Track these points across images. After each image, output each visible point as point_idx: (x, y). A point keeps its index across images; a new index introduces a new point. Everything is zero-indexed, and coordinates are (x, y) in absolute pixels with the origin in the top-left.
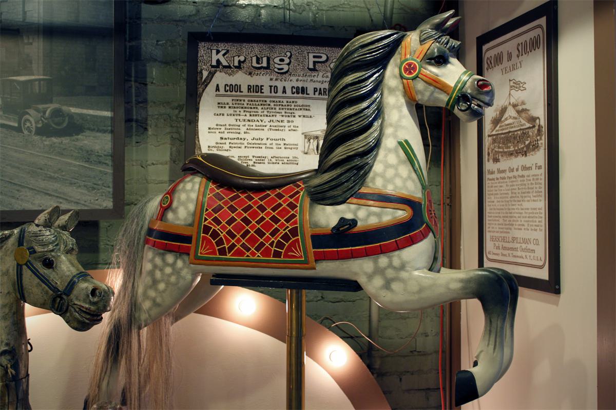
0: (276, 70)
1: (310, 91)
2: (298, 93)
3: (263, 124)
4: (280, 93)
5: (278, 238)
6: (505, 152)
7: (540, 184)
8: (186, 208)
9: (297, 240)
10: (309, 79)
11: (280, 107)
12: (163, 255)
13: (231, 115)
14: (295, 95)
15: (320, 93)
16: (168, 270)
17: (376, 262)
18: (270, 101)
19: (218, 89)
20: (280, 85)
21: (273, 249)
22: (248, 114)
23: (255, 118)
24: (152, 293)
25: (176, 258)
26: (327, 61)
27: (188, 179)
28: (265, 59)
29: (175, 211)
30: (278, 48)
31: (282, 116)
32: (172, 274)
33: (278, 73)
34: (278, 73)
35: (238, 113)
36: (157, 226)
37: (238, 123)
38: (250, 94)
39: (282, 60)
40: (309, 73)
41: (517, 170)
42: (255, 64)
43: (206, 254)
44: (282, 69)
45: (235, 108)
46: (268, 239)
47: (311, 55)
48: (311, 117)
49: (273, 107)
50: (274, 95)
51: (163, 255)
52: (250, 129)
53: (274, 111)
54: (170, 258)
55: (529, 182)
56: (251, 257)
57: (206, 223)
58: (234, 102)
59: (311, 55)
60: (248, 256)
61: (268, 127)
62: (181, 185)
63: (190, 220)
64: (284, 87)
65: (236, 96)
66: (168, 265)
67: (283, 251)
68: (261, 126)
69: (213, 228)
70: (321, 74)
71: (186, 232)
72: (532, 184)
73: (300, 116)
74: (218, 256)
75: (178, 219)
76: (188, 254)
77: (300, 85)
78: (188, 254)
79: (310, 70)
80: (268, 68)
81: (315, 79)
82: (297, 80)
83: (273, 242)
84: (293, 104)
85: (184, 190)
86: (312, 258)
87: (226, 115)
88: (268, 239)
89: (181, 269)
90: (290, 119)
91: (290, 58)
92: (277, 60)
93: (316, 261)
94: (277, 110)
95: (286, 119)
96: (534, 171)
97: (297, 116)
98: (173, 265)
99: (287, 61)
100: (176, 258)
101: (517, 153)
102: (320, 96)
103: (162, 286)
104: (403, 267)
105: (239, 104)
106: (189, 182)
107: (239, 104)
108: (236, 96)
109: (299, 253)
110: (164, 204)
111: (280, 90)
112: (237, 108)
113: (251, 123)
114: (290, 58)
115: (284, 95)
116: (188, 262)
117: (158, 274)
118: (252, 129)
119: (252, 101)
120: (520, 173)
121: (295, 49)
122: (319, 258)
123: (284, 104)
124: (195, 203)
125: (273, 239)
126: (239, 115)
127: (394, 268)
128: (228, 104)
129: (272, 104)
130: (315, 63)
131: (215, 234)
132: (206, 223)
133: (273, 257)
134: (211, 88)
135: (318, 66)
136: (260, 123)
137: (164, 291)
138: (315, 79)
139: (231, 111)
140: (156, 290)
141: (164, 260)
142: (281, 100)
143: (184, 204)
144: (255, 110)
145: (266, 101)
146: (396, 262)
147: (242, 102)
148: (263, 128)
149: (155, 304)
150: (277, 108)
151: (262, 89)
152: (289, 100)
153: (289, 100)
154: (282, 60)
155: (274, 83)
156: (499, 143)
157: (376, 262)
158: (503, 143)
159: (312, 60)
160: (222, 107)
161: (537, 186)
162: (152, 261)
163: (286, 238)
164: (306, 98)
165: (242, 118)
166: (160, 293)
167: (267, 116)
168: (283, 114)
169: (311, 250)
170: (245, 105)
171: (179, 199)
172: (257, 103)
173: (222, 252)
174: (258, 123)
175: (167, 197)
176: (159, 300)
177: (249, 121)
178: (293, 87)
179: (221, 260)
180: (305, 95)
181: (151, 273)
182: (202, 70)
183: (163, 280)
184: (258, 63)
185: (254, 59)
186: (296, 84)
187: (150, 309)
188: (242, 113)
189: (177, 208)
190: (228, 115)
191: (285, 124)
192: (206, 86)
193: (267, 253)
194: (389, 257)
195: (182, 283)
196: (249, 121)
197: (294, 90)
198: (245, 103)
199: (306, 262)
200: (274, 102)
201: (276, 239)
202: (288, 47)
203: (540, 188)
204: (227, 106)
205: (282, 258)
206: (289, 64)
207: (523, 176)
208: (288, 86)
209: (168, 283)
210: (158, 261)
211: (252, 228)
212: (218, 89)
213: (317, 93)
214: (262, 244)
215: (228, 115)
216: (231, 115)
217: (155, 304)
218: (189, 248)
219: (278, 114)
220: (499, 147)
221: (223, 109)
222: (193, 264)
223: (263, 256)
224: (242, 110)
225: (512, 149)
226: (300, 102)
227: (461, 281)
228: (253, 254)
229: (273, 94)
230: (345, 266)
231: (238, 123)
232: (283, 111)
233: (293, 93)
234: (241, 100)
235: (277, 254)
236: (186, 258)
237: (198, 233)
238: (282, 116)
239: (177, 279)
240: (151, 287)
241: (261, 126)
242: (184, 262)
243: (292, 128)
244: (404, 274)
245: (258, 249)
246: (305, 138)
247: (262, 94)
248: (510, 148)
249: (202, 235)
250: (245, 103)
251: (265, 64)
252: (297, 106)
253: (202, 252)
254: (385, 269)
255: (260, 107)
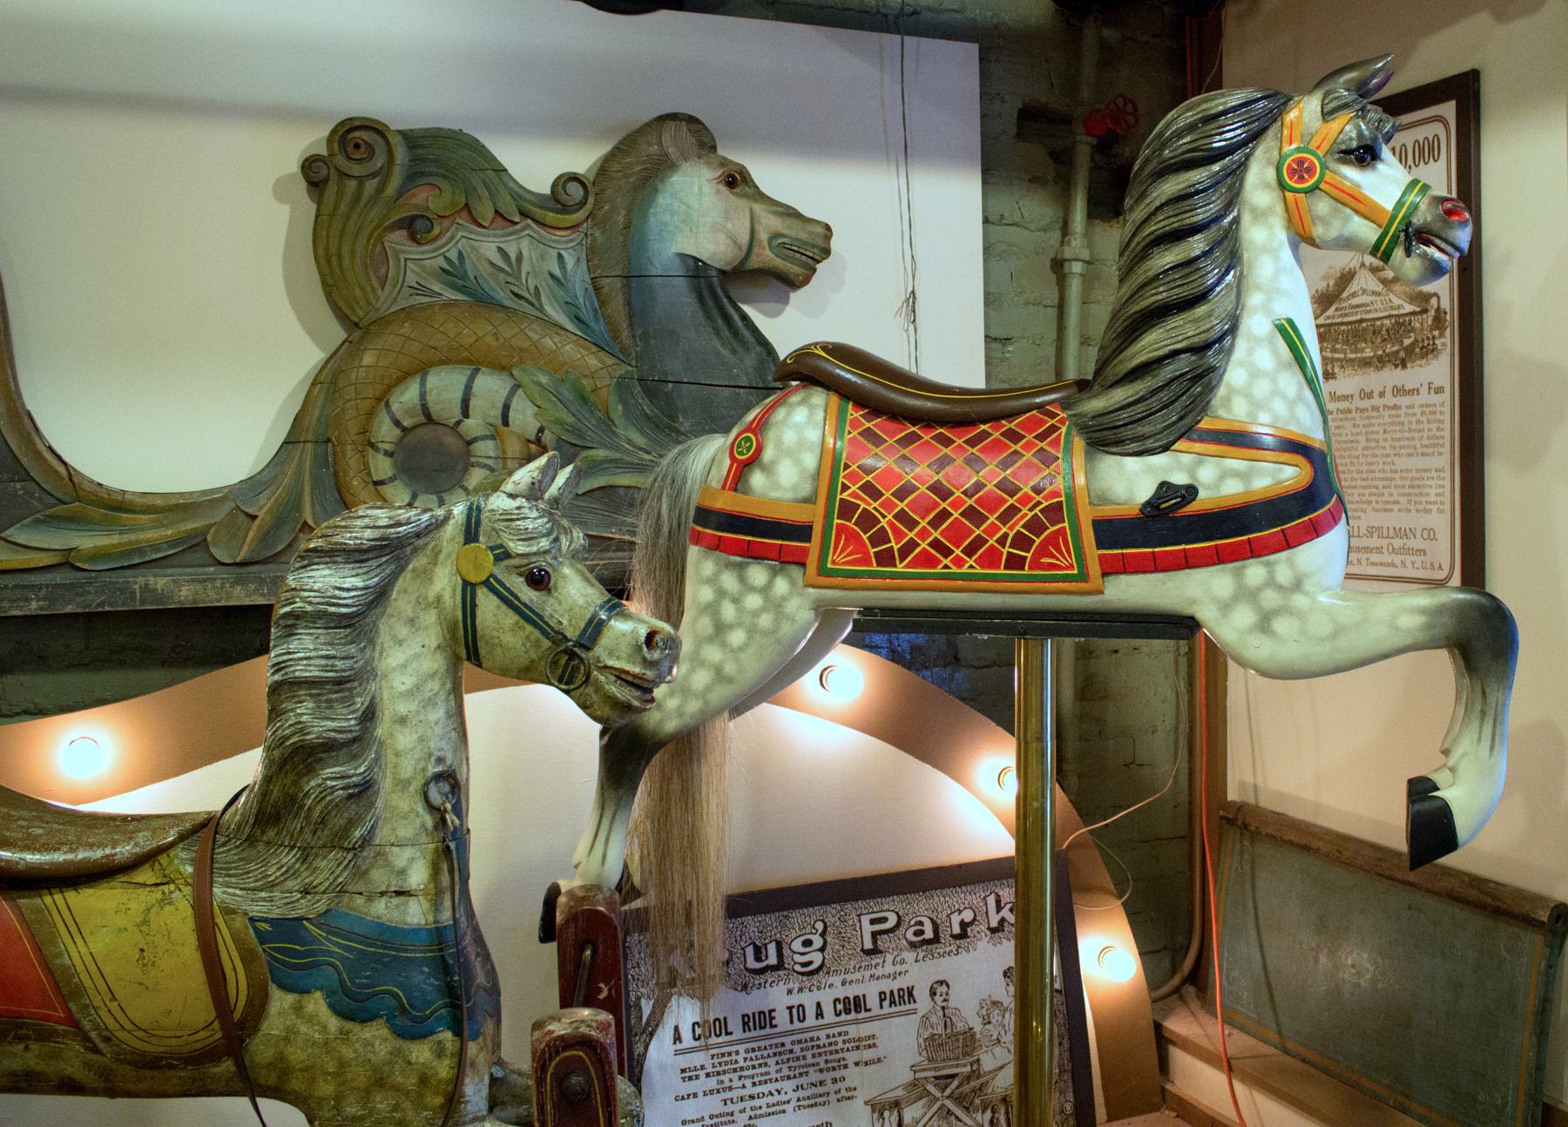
0: (798, 968)
1: (872, 1002)
2: (847, 1011)
3: (783, 1098)
4: (811, 1021)
5: (1018, 528)
6: (1352, 360)
7: (1441, 422)
8: (798, 462)
9: (1062, 531)
10: (867, 974)
11: (816, 1051)
12: (740, 567)
13: (711, 1092)
14: (843, 1017)
15: (892, 1003)
16: (753, 601)
17: (1238, 575)
18: (793, 1043)
19: (677, 1038)
20: (808, 1000)
21: (1005, 551)
22: (748, 1082)
23: (764, 1089)
24: (713, 654)
25: (774, 573)
26: (898, 925)
27: (795, 398)
28: (772, 948)
29: (768, 470)
30: (797, 917)
31: (821, 1071)
32: (764, 609)
33: (803, 974)
34: (803, 974)
35: (727, 1084)
36: (725, 502)
37: (730, 1108)
38: (748, 1035)
39: (807, 943)
40: (867, 960)
41: (1382, 395)
42: (752, 963)
43: (847, 563)
44: (810, 963)
45: (718, 1073)
46: (993, 529)
47: (866, 920)
48: (879, 1060)
49: (799, 1053)
50: (797, 1025)
51: (740, 567)
52: (756, 1117)
53: (802, 1062)
54: (758, 574)
55: (1413, 419)
56: (954, 570)
57: (845, 495)
58: (716, 1061)
59: (866, 920)
60: (946, 567)
61: (794, 1103)
62: (781, 413)
63: (806, 489)
64: (818, 1005)
65: (719, 1046)
66: (753, 589)
67: (1029, 555)
68: (778, 1104)
69: (863, 505)
70: (889, 958)
71: (798, 515)
72: (1418, 422)
73: (857, 1064)
74: (875, 568)
75: (778, 487)
76: (803, 565)
77: (851, 992)
78: (803, 565)
79: (868, 953)
80: (780, 966)
81: (879, 971)
82: (844, 983)
83: (1006, 536)
84: (840, 1040)
85: (783, 451)
86: (1094, 568)
87: (701, 1094)
88: (993, 529)
89: (784, 599)
90: (837, 1074)
91: (823, 934)
92: (797, 945)
93: (1105, 574)
94: (810, 1060)
95: (828, 1076)
96: (1425, 397)
97: (851, 1065)
98: (765, 590)
99: (818, 942)
100: (774, 573)
101: (1381, 362)
102: (894, 1009)
103: (737, 637)
104: (1297, 585)
105: (726, 1063)
106: (799, 404)
107: (726, 1063)
108: (719, 1046)
109: (1067, 561)
110: (741, 453)
111: (811, 1011)
112: (725, 1072)
113: (757, 1103)
114: (823, 934)
115: (821, 1022)
116: (800, 583)
117: (728, 611)
118: (761, 1116)
119: (753, 1050)
120: (1389, 400)
121: (831, 913)
122: (1112, 568)
123: (821, 1043)
124: (818, 451)
125: (1005, 529)
126: (730, 1088)
127: (1280, 588)
128: (703, 1067)
129: (797, 1048)
130: (874, 935)
131: (868, 520)
132: (845, 495)
133: (1006, 568)
134: (664, 1035)
135: (883, 942)
136: (777, 1098)
137: (741, 649)
138: (879, 971)
139: (712, 1083)
140: (724, 645)
141: (742, 579)
142: (815, 1034)
143: (791, 453)
144: (763, 1070)
145: (783, 1045)
146: (1283, 575)
147: (734, 1057)
148: (784, 1107)
149: (719, 675)
150: (809, 1054)
151: (772, 1018)
152: (831, 1031)
153: (831, 1031)
154: (807, 943)
155: (795, 1000)
156: (1336, 341)
157: (1238, 575)
158: (1346, 342)
159: (868, 929)
160: (690, 1078)
161: (1433, 426)
162: (712, 581)
163: (1035, 526)
164: (865, 1021)
165: (735, 1094)
166: (732, 651)
167: (789, 1078)
168: (823, 1065)
169: (1093, 553)
170: (742, 1064)
171: (779, 443)
172: (765, 1053)
173: (886, 558)
174: (771, 1100)
175: (748, 439)
176: (730, 668)
177: (752, 1097)
178: (837, 1000)
179: (883, 576)
180: (863, 1015)
181: (712, 609)
182: (639, 999)
183: (739, 624)
184: (758, 959)
185: (750, 951)
186: (841, 993)
187: (709, 688)
188: (737, 1083)
189: (773, 462)
190: (705, 1094)
191: (830, 1087)
192: (652, 1034)
193: (991, 559)
194: (1268, 564)
195: (786, 629)
196: (752, 1097)
197: (840, 1007)
198: (740, 1058)
199: (1083, 576)
200: (800, 1042)
201: (1011, 528)
202: (816, 912)
203: (1439, 429)
204: (702, 1073)
205: (1026, 571)
206: (822, 949)
207: (1395, 407)
208: (826, 998)
209: (752, 631)
210: (729, 581)
211: (955, 505)
212: (677, 1038)
213: (886, 1004)
214: (980, 542)
215: (705, 1094)
216: (711, 1092)
217: (719, 675)
218: (805, 552)
219: (811, 1070)
220: (1334, 350)
221: (695, 1082)
222: (814, 586)
223: (983, 567)
224: (735, 1076)
225: (1368, 353)
226: (853, 1031)
227: (1423, 611)
228: (959, 562)
229: (797, 1025)
230: (1170, 584)
231: (730, 1108)
232: (821, 1060)
233: (838, 1014)
234: (730, 1054)
235: (1015, 562)
236: (796, 571)
237: (828, 517)
238: (821, 1071)
239: (776, 620)
240: (710, 640)
241: (778, 1104)
242: (793, 582)
243: (844, 1093)
244: (1299, 601)
245: (970, 551)
246: (873, 1111)
247: (774, 1030)
248: (1362, 351)
249: (836, 521)
250: (740, 1058)
251: (773, 960)
252: (849, 1041)
253: (837, 559)
254: (1259, 589)
255: (771, 1061)
